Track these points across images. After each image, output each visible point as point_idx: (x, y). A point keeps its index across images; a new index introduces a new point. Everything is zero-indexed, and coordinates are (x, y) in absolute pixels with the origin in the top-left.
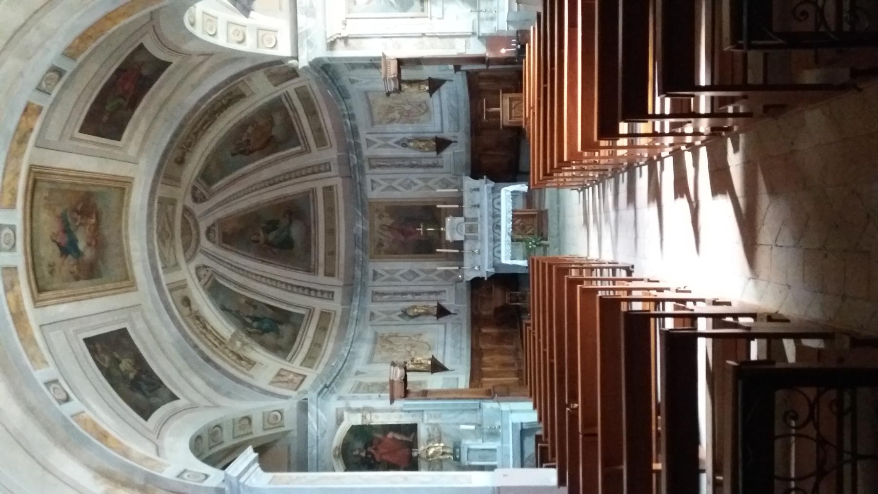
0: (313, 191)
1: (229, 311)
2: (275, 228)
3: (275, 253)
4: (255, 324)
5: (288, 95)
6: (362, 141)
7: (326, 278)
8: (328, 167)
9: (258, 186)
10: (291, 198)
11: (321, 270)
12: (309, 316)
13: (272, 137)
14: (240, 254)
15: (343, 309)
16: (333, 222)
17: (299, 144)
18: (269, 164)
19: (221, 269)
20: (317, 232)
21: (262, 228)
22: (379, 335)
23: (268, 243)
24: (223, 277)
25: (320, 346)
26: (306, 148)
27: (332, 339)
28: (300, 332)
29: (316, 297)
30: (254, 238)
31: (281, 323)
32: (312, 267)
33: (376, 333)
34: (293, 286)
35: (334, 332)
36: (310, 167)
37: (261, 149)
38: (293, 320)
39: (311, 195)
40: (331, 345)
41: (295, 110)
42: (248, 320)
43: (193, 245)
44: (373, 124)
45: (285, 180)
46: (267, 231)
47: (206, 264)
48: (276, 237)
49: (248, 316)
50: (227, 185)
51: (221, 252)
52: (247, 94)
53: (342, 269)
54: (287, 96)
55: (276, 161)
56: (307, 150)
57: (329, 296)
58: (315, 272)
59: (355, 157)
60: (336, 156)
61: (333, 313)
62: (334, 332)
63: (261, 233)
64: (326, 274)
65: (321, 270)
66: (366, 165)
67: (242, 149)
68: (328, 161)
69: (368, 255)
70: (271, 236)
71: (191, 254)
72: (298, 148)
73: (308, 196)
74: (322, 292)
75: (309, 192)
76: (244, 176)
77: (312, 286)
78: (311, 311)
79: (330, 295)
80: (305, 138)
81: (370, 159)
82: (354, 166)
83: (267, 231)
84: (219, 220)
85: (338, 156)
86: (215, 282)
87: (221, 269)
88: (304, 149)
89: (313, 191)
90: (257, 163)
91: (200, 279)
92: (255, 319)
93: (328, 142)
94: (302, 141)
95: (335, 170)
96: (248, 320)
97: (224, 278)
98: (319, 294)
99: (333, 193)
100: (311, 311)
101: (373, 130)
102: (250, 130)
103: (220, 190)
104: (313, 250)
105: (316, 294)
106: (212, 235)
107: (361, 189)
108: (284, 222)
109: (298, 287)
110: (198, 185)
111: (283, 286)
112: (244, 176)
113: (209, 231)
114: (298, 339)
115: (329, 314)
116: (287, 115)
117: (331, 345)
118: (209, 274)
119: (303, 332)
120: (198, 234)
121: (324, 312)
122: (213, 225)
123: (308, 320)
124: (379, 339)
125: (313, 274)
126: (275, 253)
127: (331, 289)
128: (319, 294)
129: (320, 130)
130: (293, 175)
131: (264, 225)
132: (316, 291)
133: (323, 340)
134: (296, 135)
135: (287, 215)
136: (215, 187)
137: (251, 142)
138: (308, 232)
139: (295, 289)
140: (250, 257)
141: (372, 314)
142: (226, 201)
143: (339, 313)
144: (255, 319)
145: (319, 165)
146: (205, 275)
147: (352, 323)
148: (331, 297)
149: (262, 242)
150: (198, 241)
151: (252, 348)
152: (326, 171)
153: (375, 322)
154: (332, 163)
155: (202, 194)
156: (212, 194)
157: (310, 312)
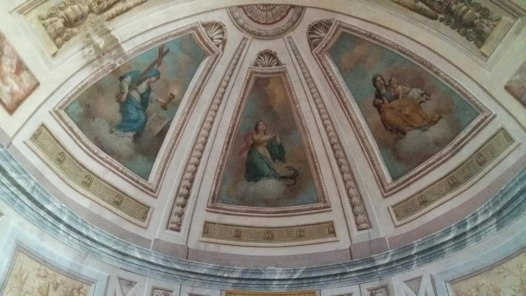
0: (327, 208)
1: (158, 62)
2: (274, 157)
3: (241, 153)
4: (136, 96)
5: (491, 120)
6: (415, 271)
7: (203, 223)
8: (364, 226)
9: (330, 128)
10: (315, 176)
11: (214, 218)
12: (143, 185)
13: (404, 133)
14: (241, 103)
15: (150, 241)
16: (282, 239)
17: (394, 179)
18: (361, 140)
19: (220, 69)
20: (269, 215)
21: (275, 138)
22: (85, 287)
23: (254, 146)
24: (209, 70)
25: (87, 184)
26: (390, 190)
27: (96, 209)
28: (116, 163)
29: (174, 204)
30: (261, 127)
31: (137, 137)
32: (220, 205)
33: (90, 282)
34: (194, 173)
35: (109, 216)
36: (361, 199)
37: (384, 121)
38: (140, 159)
39: (321, 205)
40: (85, 203)
41: (456, 151)
42: (143, 87)
43: (254, 27)
44: (452, 282)
45: (340, 166)
46: (270, 145)
47: (227, 46)
48: (261, 157)
49: (149, 90)
50: (329, 79)
51: (243, 74)
52: (484, 49)
53: (212, 248)
54: (490, 118)
55: (366, 150)
56: (386, 193)
57: (173, 223)
58: (213, 207)
59: (387, 260)
60: (382, 236)
61: (144, 224)
62: (109, 216)
63: (268, 137)
64: (207, 225)
65: (214, 218)
66: (375, 284)
67: (384, 91)
68: (373, 224)
69: (231, 289)
70: (262, 150)
71: (241, 21)
72: (388, 179)
73: (318, 201)
74: (181, 215)
75: (325, 202)
76: (344, 105)
77: (191, 201)
78: (153, 192)
79: (174, 226)
80: (407, 184)
81: (386, 287)
82: (372, 260)
83: (270, 145)
84: (284, 73)
85: (383, 239)
86: (205, 55)
87: (220, 69)
88: (387, 188)
89: (327, 208)
90: (363, 122)
91: (206, 26)
92: (145, 101)
93: (404, 221)
94: (400, 181)
95: (360, 237)
96: (143, 87)
97: (209, 71)
98: (178, 209)
99: (324, 236)
100: (153, 192)
101: (440, 284)
102: (415, 93)
103: (324, 69)
104: (245, 208)
105: (178, 205)
106: (266, 60)
107: (336, 275)
108: (281, 168)
109: (192, 181)
110: (332, 29)
111: (194, 160)
112: (344, 105)
113: (270, 55)
114: (104, 155)
115: (144, 218)
116: (446, 142)
117: (85, 203)
118: (212, 45)
119: (117, 169)
120: (268, 37)
121: (146, 213)
122: (279, 64)
123: (137, 182)
124: (78, 284)
125: (209, 205)
126: (241, 153)
127: (184, 227)
128: (178, 209)
129: (424, 203)
130: (347, 176)
131: (278, 140)
132: (184, 206)
133: (94, 194)
134: (410, 170)
135: (292, 172)
136: (329, 61)
137: (394, 103)
138: (268, 203)
139: (188, 175)
140: (236, 117)
141: (131, 284)
142: (309, 80)
143: (141, 233)
144: (145, 101)
145: (365, 212)
146: (212, 39)
147: (116, 243)
148: (171, 226)
149: (256, 137)
150: (258, 36)
151: (90, 63)
152: (357, 224)
153: (115, 285)
154: (371, 230)
155: (321, 39)
156: (319, 60)
157: (152, 191)
